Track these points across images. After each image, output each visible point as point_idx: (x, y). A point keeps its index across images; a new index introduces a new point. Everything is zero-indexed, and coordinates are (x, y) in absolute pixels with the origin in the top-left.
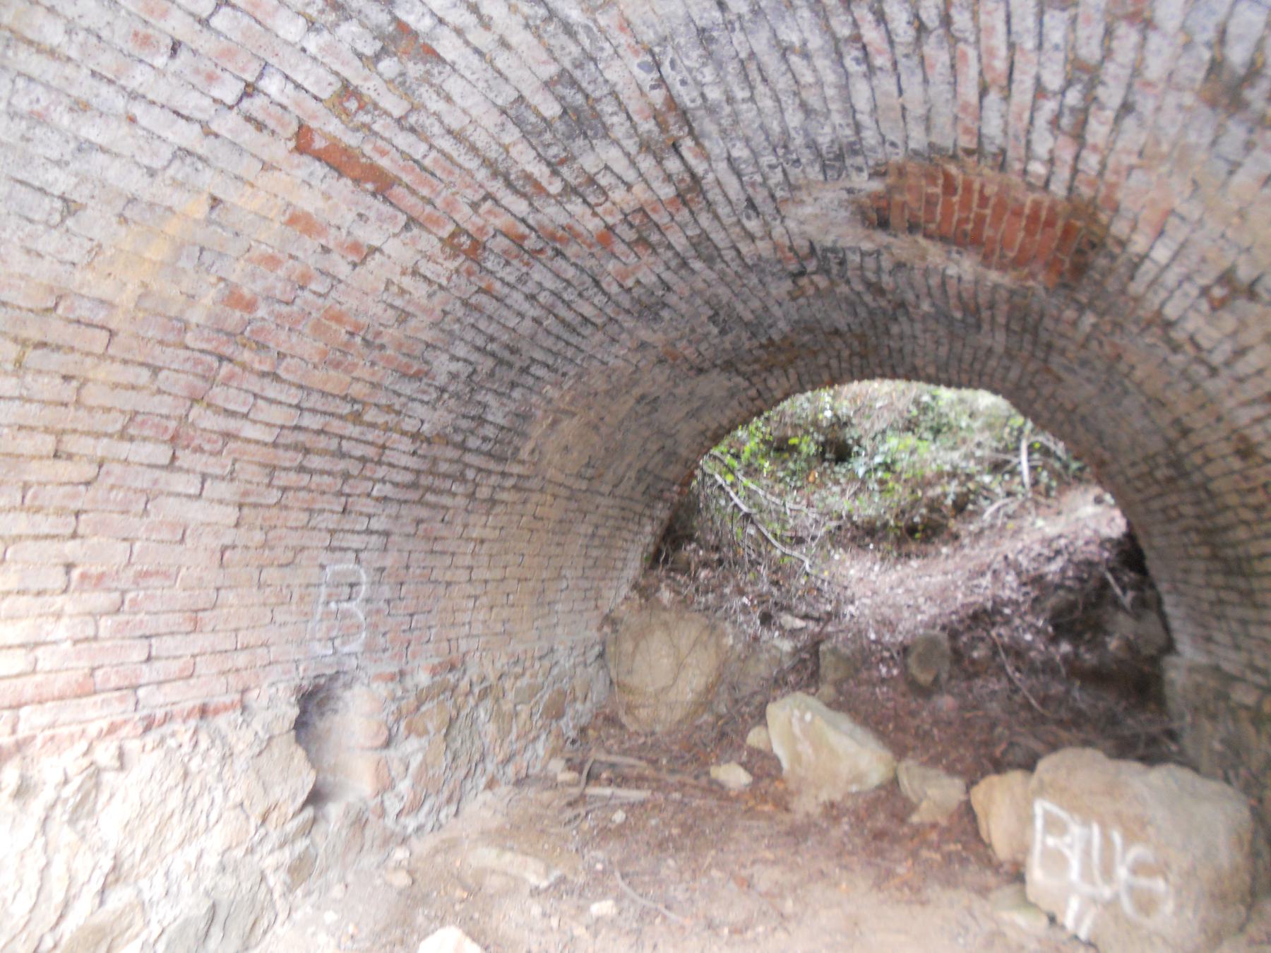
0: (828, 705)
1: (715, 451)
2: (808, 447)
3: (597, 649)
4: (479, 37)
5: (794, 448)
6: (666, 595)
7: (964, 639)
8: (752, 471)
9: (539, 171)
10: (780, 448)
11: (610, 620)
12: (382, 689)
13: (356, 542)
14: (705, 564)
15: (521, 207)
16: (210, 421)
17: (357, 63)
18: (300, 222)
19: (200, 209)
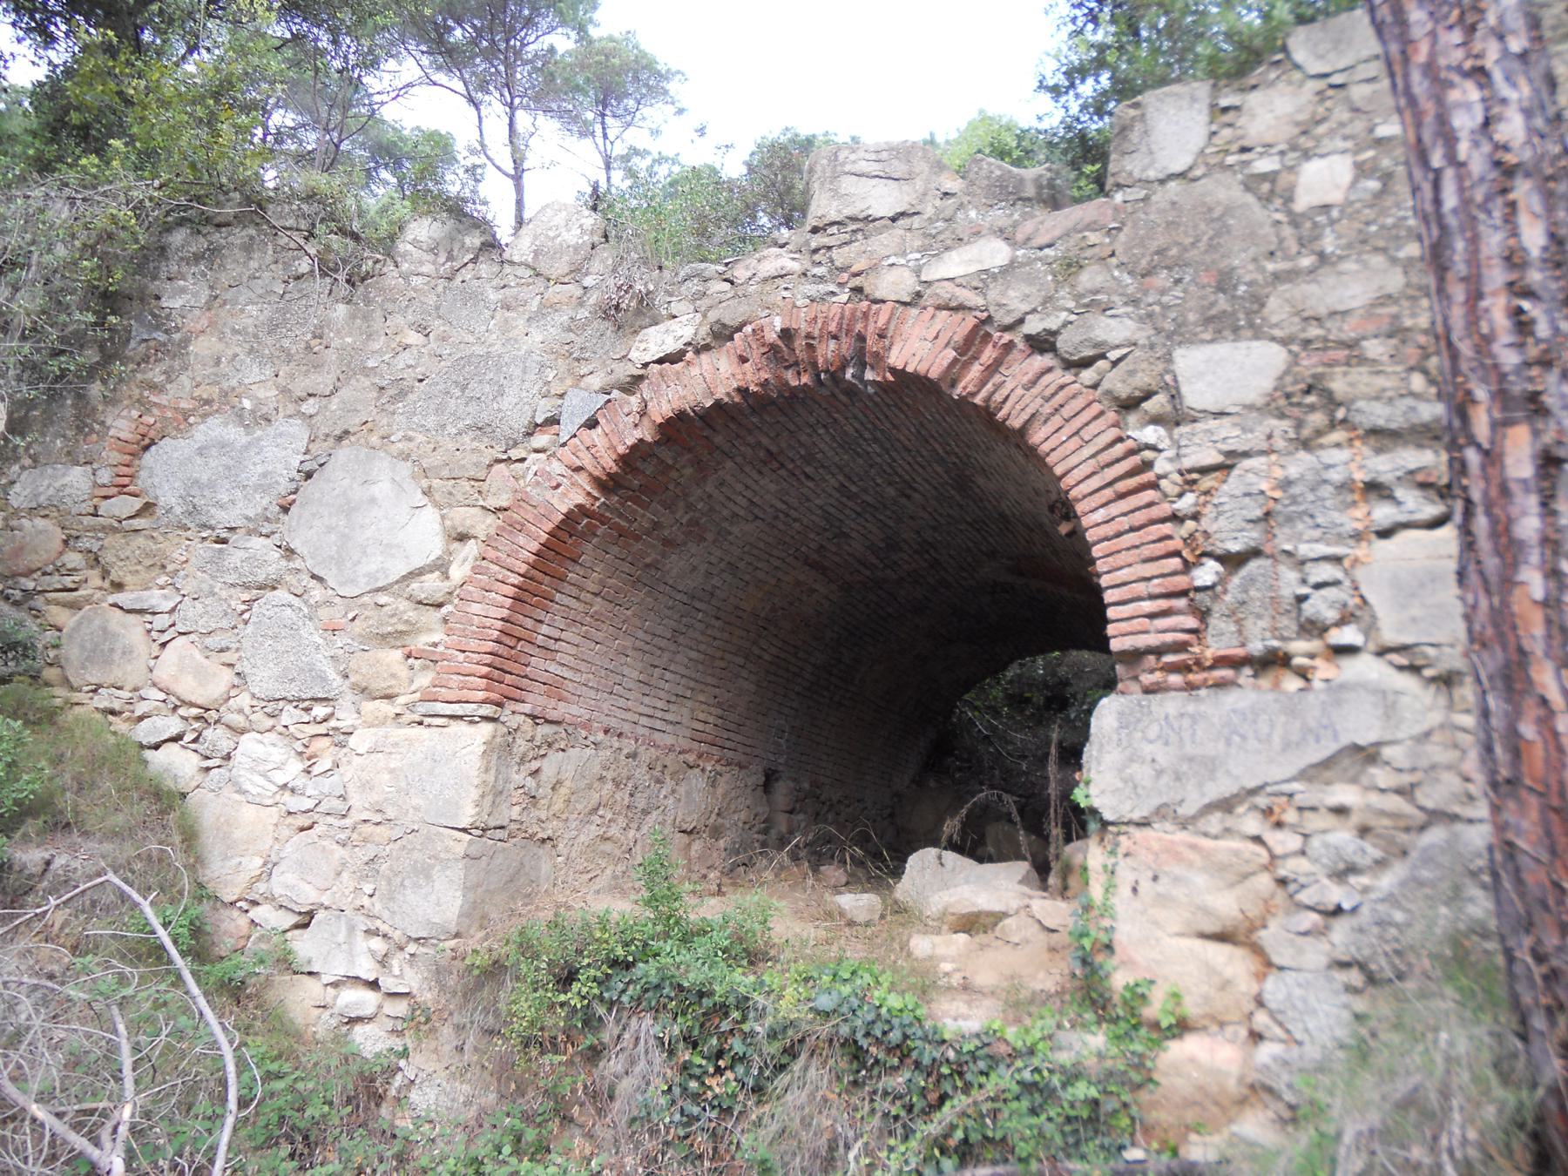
0: (808, 144)
1: (966, 697)
2: (1038, 699)
3: (889, 811)
4: (748, 493)
5: (1028, 700)
6: (932, 784)
7: (526, 12)
8: (996, 713)
9: (875, 561)
10: (1018, 701)
11: (897, 795)
12: (792, 784)
13: (786, 711)
14: (960, 769)
15: (868, 573)
16: (757, 651)
17: (1250, 526)
18: (798, 583)
19: (774, 582)
